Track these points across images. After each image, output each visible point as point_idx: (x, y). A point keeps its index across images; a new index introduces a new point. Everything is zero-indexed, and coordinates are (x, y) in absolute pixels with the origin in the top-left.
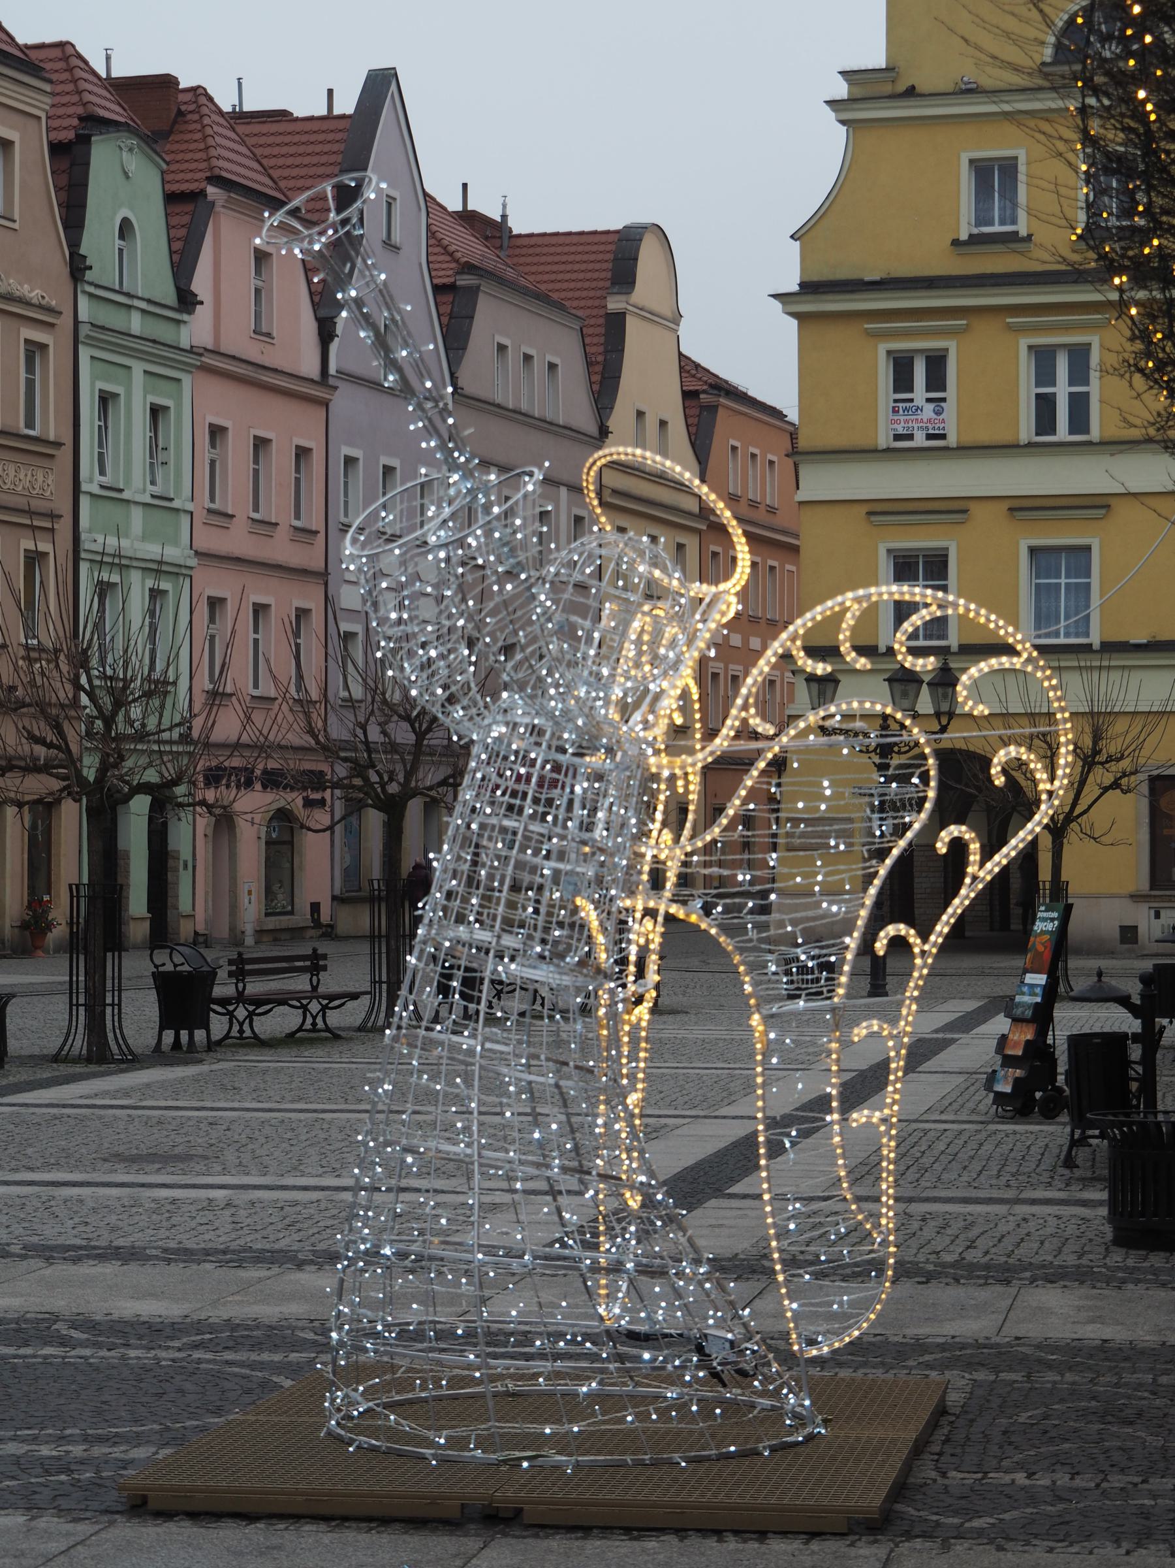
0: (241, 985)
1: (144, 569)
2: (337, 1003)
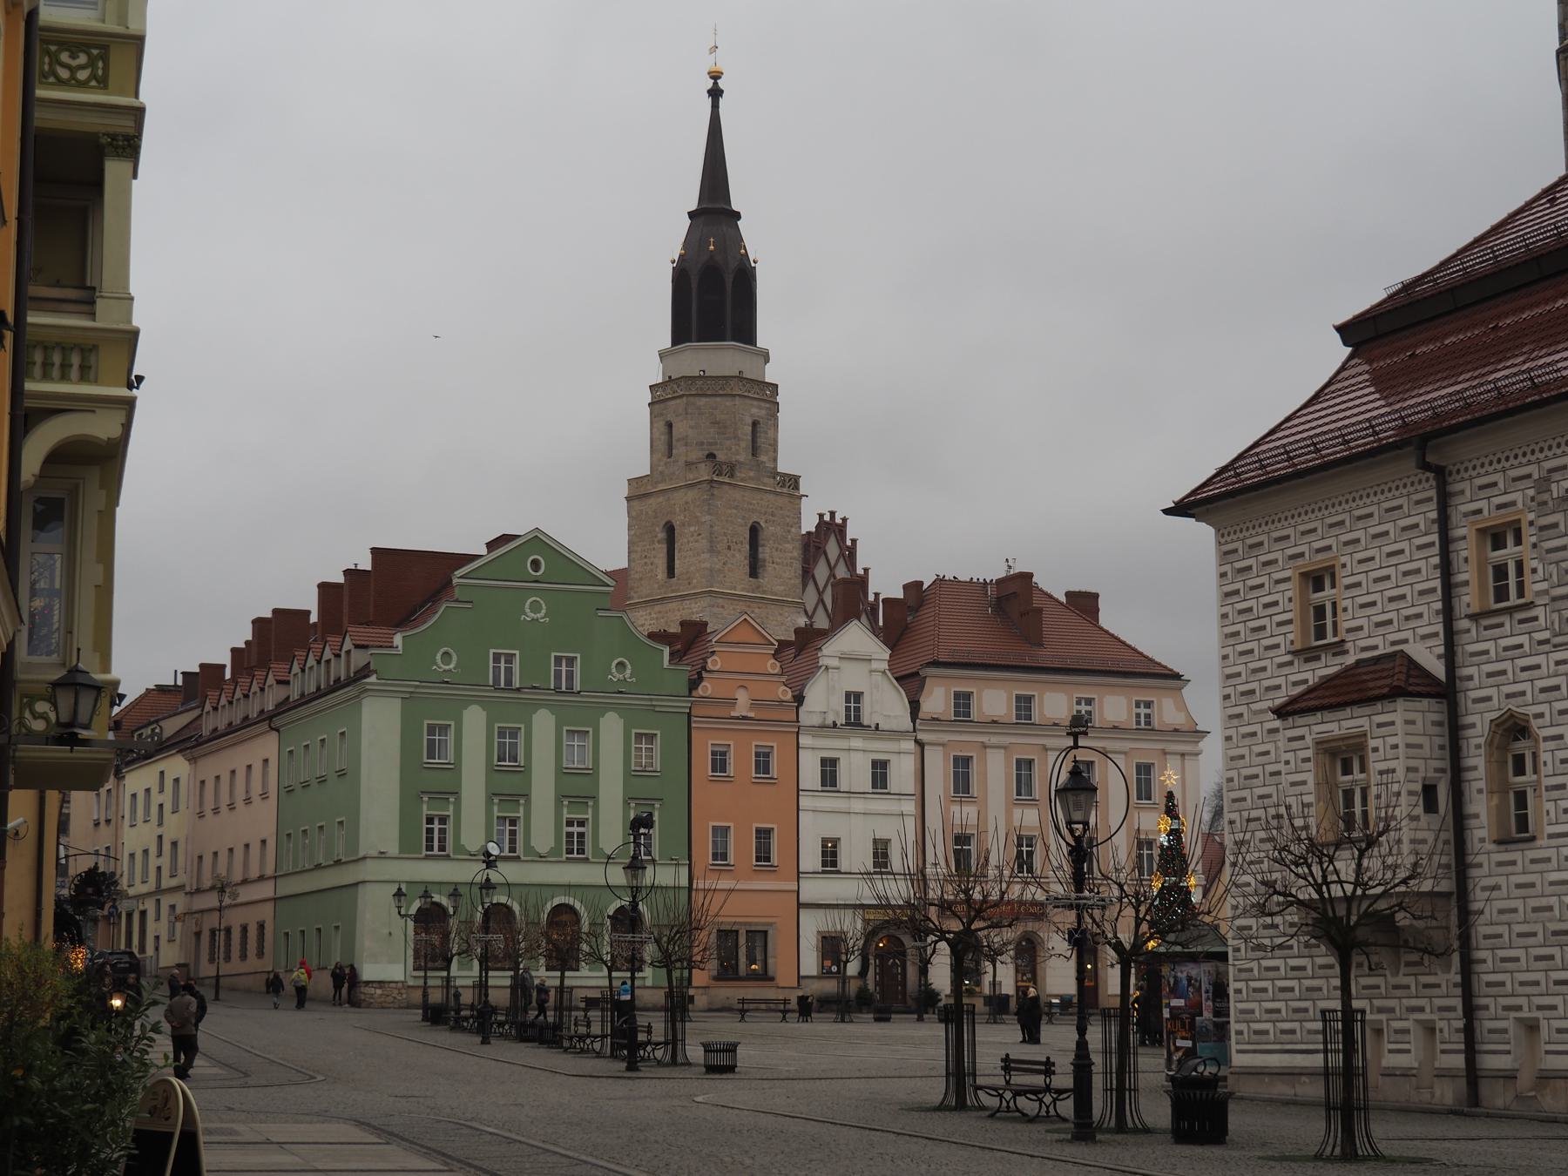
0: (1048, 1080)
2: (1065, 1096)
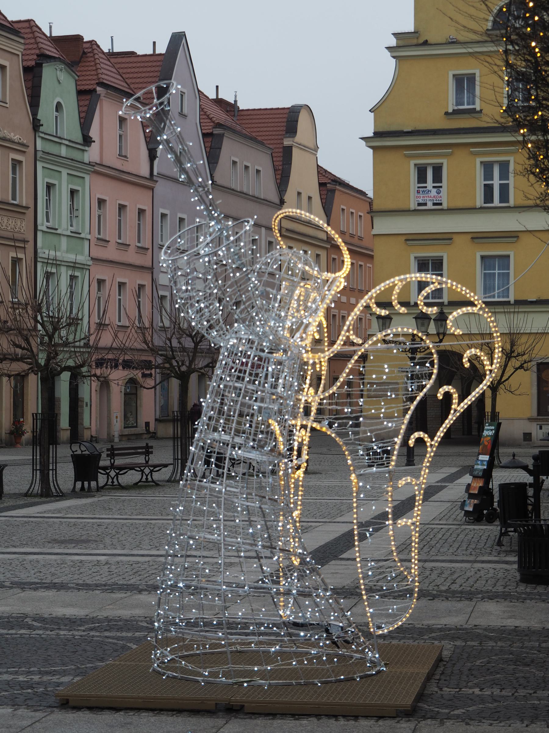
0: (112, 461)
1: (67, 266)
2: (157, 469)
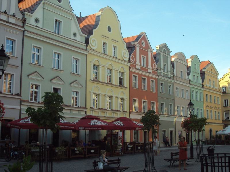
2: (176, 161)
